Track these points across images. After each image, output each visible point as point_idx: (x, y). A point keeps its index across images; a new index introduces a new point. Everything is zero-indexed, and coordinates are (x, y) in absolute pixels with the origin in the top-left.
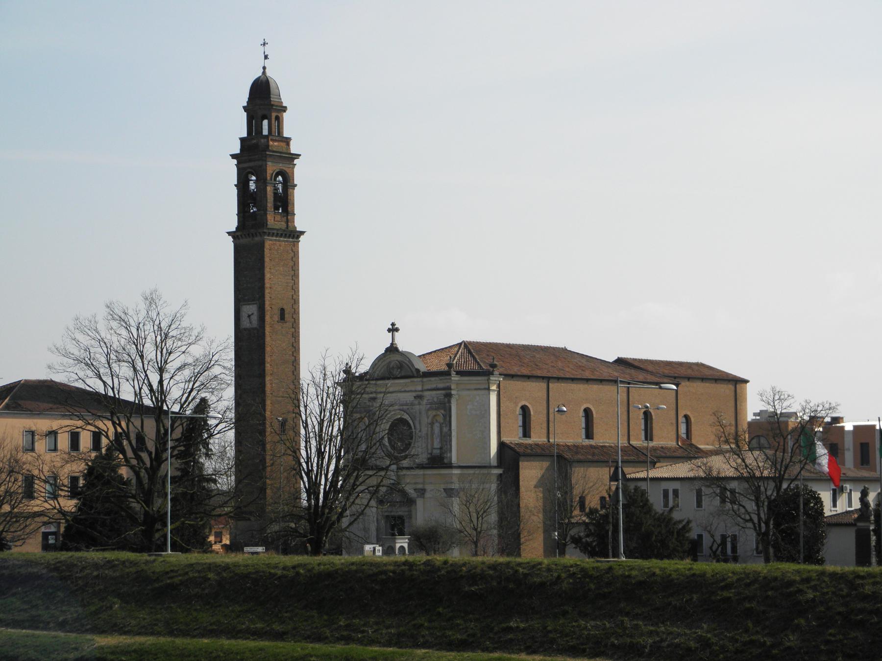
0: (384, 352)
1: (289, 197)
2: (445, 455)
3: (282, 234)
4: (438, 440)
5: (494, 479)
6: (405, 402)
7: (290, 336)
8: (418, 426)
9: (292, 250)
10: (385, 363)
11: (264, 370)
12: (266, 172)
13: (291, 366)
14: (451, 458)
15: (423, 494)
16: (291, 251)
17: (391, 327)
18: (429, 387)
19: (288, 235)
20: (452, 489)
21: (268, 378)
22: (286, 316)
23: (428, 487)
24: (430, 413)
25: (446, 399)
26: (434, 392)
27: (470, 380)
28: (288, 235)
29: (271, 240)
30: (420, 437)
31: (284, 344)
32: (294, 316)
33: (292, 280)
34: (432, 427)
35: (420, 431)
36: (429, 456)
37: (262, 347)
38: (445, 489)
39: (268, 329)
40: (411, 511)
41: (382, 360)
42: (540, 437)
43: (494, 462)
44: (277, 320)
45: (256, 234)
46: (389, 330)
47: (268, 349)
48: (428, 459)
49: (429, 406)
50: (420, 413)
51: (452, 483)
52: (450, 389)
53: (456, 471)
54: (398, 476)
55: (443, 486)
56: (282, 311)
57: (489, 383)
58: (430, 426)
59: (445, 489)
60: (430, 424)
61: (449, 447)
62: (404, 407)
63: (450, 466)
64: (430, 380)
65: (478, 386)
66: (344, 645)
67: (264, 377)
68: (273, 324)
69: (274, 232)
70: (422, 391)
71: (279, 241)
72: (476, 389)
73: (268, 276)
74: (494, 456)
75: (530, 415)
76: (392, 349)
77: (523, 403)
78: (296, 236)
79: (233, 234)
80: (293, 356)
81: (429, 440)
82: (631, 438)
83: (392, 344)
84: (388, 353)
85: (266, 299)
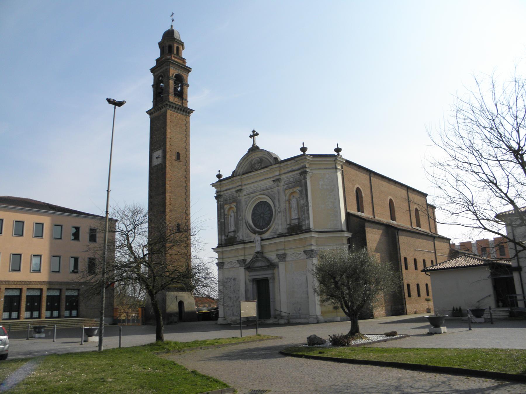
0: (247, 152)
1: (184, 90)
2: (304, 223)
3: (178, 109)
4: (296, 212)
5: (345, 241)
6: (265, 188)
7: (183, 170)
8: (277, 204)
9: (185, 120)
10: (247, 162)
11: (165, 189)
12: (169, 72)
13: (184, 189)
14: (309, 224)
15: (285, 258)
16: (184, 120)
17: (252, 134)
18: (286, 171)
19: (182, 110)
20: (312, 250)
21: (167, 195)
22: (181, 158)
23: (288, 252)
24: (287, 191)
25: (302, 176)
26: (291, 174)
27: (320, 161)
28: (182, 110)
29: (171, 110)
30: (279, 212)
31: (179, 175)
32: (186, 159)
33: (185, 137)
34: (290, 204)
35: (279, 207)
36: (288, 226)
37: (164, 175)
38: (304, 251)
39: (168, 163)
40: (274, 274)
41: (246, 160)
42: (369, 214)
43: (344, 228)
44: (175, 159)
45: (162, 107)
46: (251, 136)
47: (168, 176)
48: (288, 229)
49: (286, 186)
50: (279, 193)
51: (312, 245)
52: (306, 167)
53: (314, 235)
54: (262, 246)
55: (303, 249)
56: (178, 154)
57: (335, 164)
58: (287, 202)
59: (304, 251)
60: (288, 200)
61: (306, 215)
62: (265, 191)
63: (309, 231)
64: (287, 164)
65: (327, 166)
66: (252, 160)
67: (165, 193)
68: (172, 161)
69: (171, 104)
70: (279, 175)
71: (177, 112)
72: (325, 169)
73: (168, 131)
74: (344, 222)
75: (362, 196)
76: (254, 149)
77: (357, 186)
78: (188, 112)
79: (149, 112)
80: (185, 183)
81: (288, 214)
82: (413, 225)
83: (253, 145)
84: (251, 152)
85: (167, 144)
